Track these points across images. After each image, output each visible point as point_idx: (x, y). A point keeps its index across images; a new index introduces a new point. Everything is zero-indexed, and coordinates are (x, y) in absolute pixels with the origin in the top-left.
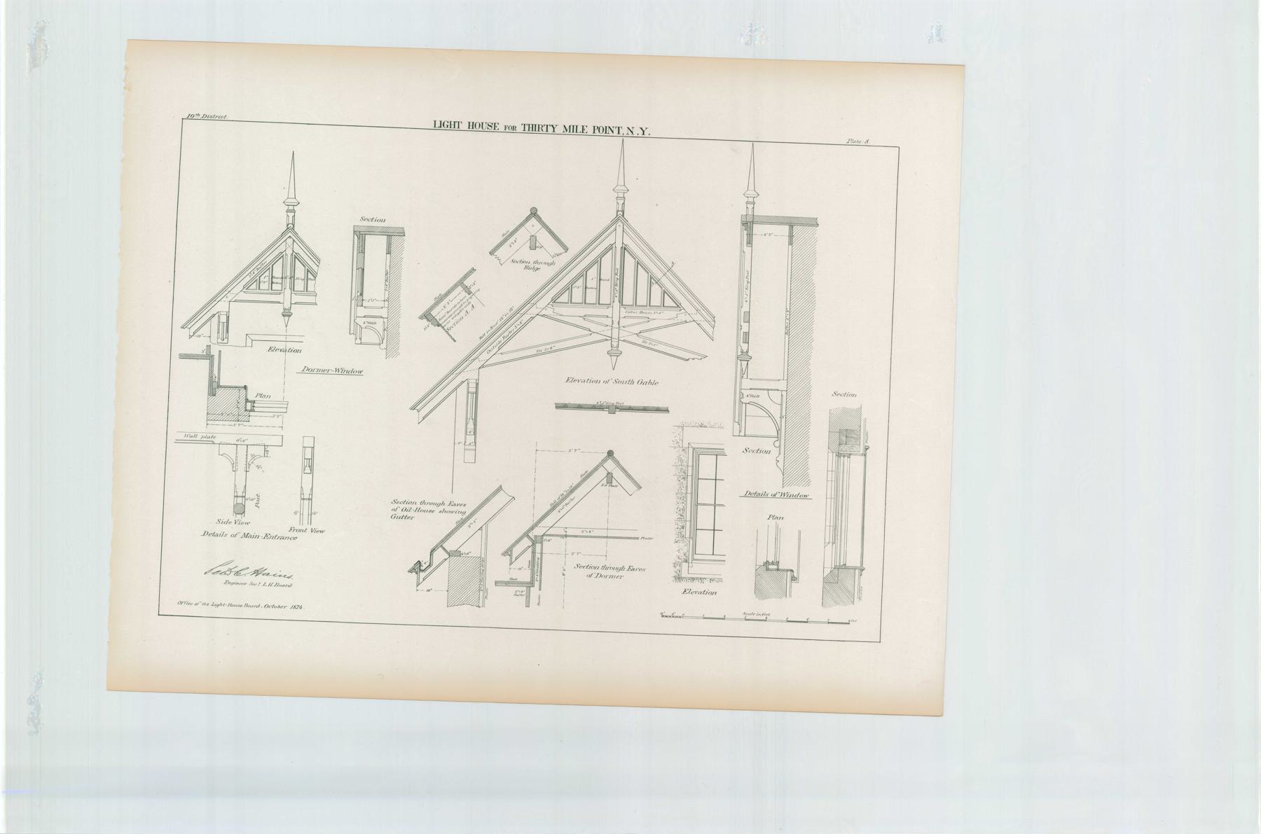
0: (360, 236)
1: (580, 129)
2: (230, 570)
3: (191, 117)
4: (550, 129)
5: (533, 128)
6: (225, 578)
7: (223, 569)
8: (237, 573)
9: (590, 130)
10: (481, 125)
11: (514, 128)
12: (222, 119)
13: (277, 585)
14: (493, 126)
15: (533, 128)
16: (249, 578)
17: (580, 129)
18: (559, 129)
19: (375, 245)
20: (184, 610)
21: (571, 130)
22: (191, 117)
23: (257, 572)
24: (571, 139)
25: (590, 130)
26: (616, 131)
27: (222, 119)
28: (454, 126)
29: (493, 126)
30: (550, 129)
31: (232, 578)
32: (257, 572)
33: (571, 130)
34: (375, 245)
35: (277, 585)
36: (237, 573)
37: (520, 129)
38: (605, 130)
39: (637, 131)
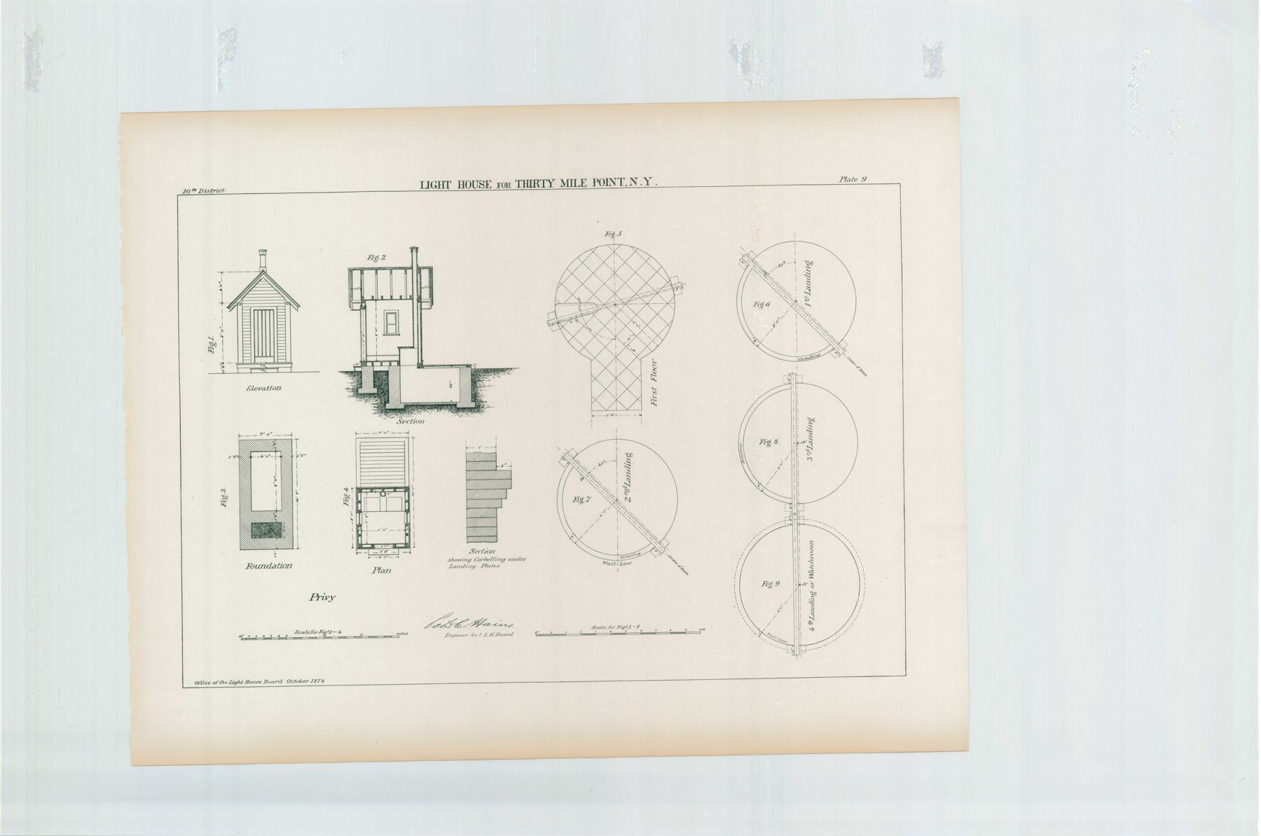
0: (351, 271)
1: (579, 183)
2: (451, 623)
3: (186, 193)
4: (547, 184)
5: (530, 184)
6: (446, 630)
7: (443, 622)
8: (458, 625)
9: (589, 183)
10: (472, 184)
11: (507, 185)
12: (219, 192)
13: (499, 634)
14: (485, 185)
15: (530, 184)
16: (467, 629)
19: (356, 274)
21: (568, 184)
22: (186, 193)
23: (477, 623)
24: (528, 194)
25: (589, 183)
26: (618, 182)
27: (219, 192)
28: (443, 185)
29: (485, 185)
30: (547, 184)
31: (453, 630)
32: (477, 623)
33: (568, 184)
34: (356, 274)
35: (499, 634)
36: (458, 625)
38: (606, 182)
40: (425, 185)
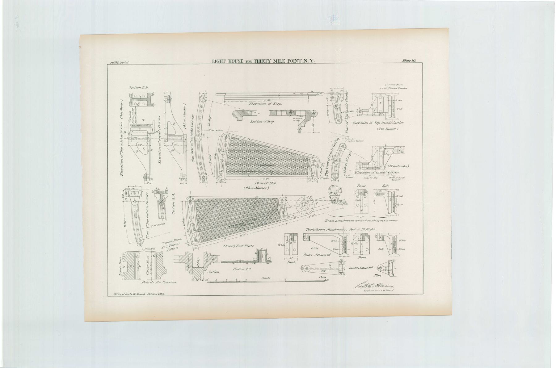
1: (281, 61)
2: (366, 285)
3: (112, 63)
4: (268, 61)
5: (259, 61)
6: (364, 289)
7: (363, 285)
8: (369, 286)
9: (286, 61)
10: (235, 61)
11: (250, 62)
12: (126, 63)
13: (387, 290)
15: (259, 61)
17: (281, 61)
18: (272, 61)
20: (264, 280)
21: (277, 61)
22: (112, 63)
23: (378, 285)
24: (278, 66)
25: (286, 61)
26: (299, 61)
27: (126, 63)
28: (221, 61)
30: (268, 61)
31: (367, 289)
32: (378, 285)
33: (277, 61)
35: (387, 290)
36: (369, 286)
37: (253, 62)
39: (308, 61)
40: (214, 61)
